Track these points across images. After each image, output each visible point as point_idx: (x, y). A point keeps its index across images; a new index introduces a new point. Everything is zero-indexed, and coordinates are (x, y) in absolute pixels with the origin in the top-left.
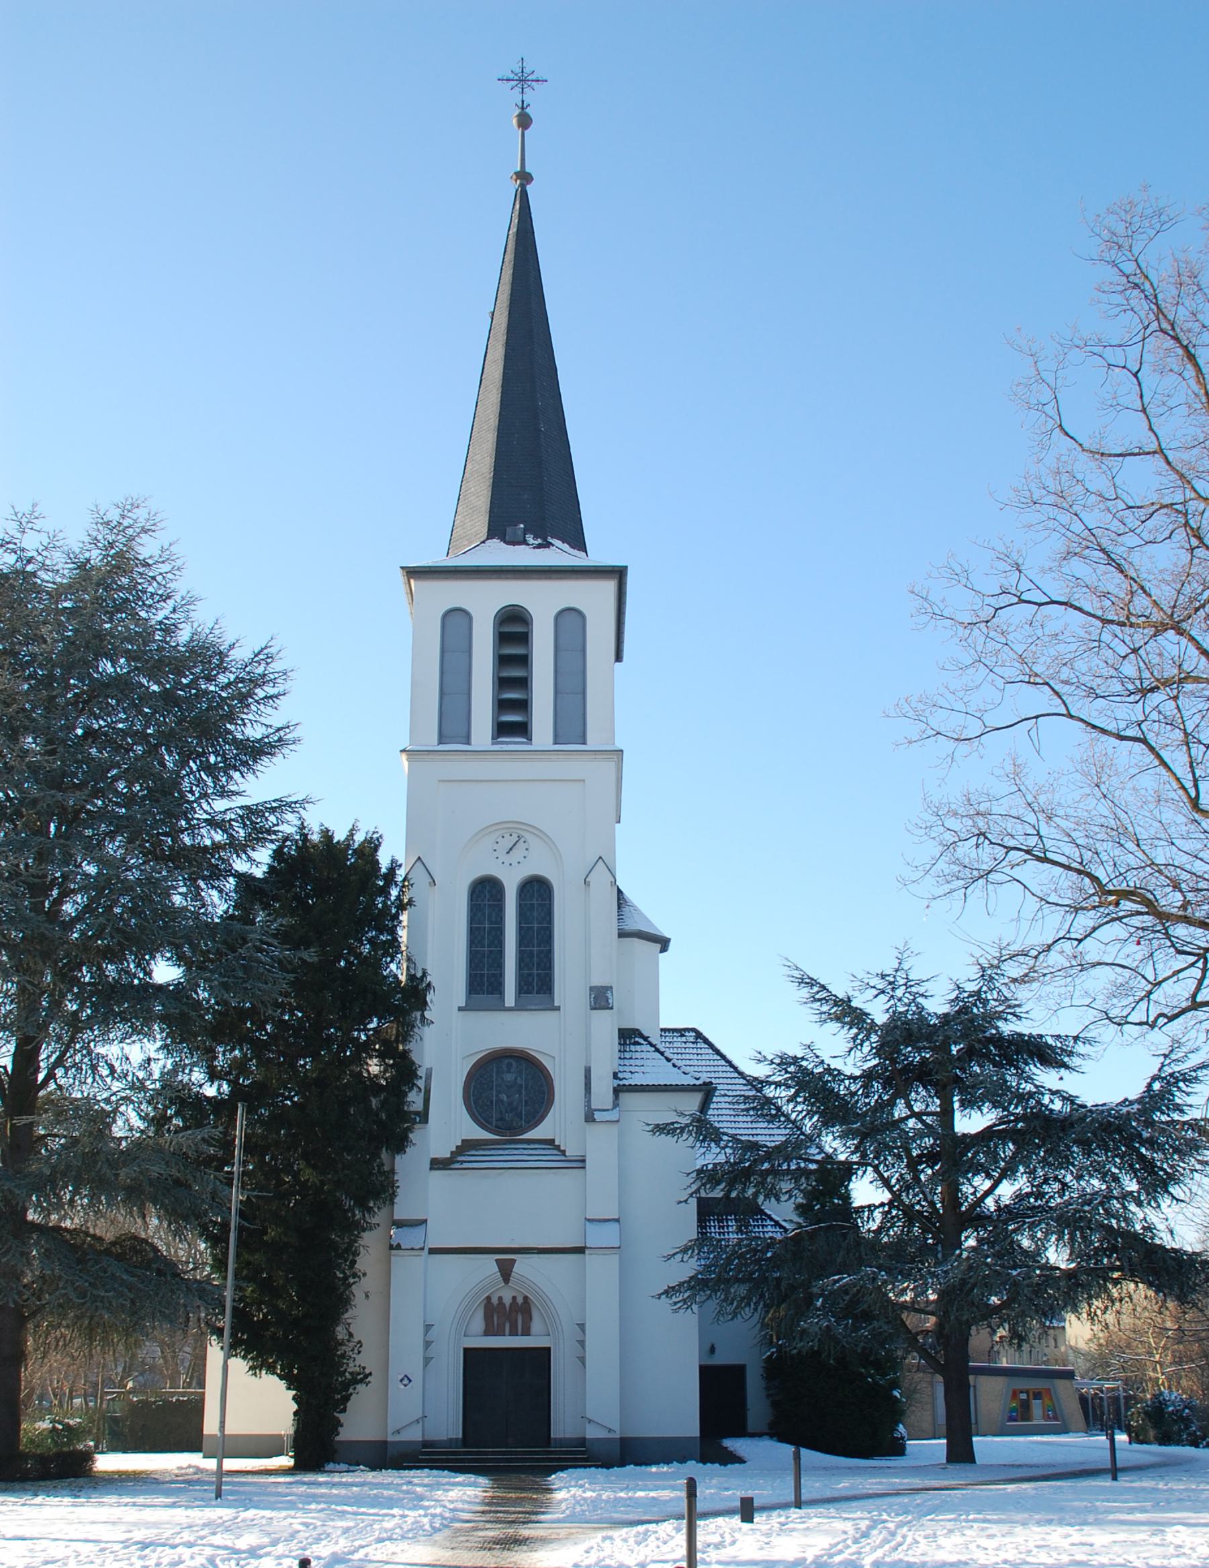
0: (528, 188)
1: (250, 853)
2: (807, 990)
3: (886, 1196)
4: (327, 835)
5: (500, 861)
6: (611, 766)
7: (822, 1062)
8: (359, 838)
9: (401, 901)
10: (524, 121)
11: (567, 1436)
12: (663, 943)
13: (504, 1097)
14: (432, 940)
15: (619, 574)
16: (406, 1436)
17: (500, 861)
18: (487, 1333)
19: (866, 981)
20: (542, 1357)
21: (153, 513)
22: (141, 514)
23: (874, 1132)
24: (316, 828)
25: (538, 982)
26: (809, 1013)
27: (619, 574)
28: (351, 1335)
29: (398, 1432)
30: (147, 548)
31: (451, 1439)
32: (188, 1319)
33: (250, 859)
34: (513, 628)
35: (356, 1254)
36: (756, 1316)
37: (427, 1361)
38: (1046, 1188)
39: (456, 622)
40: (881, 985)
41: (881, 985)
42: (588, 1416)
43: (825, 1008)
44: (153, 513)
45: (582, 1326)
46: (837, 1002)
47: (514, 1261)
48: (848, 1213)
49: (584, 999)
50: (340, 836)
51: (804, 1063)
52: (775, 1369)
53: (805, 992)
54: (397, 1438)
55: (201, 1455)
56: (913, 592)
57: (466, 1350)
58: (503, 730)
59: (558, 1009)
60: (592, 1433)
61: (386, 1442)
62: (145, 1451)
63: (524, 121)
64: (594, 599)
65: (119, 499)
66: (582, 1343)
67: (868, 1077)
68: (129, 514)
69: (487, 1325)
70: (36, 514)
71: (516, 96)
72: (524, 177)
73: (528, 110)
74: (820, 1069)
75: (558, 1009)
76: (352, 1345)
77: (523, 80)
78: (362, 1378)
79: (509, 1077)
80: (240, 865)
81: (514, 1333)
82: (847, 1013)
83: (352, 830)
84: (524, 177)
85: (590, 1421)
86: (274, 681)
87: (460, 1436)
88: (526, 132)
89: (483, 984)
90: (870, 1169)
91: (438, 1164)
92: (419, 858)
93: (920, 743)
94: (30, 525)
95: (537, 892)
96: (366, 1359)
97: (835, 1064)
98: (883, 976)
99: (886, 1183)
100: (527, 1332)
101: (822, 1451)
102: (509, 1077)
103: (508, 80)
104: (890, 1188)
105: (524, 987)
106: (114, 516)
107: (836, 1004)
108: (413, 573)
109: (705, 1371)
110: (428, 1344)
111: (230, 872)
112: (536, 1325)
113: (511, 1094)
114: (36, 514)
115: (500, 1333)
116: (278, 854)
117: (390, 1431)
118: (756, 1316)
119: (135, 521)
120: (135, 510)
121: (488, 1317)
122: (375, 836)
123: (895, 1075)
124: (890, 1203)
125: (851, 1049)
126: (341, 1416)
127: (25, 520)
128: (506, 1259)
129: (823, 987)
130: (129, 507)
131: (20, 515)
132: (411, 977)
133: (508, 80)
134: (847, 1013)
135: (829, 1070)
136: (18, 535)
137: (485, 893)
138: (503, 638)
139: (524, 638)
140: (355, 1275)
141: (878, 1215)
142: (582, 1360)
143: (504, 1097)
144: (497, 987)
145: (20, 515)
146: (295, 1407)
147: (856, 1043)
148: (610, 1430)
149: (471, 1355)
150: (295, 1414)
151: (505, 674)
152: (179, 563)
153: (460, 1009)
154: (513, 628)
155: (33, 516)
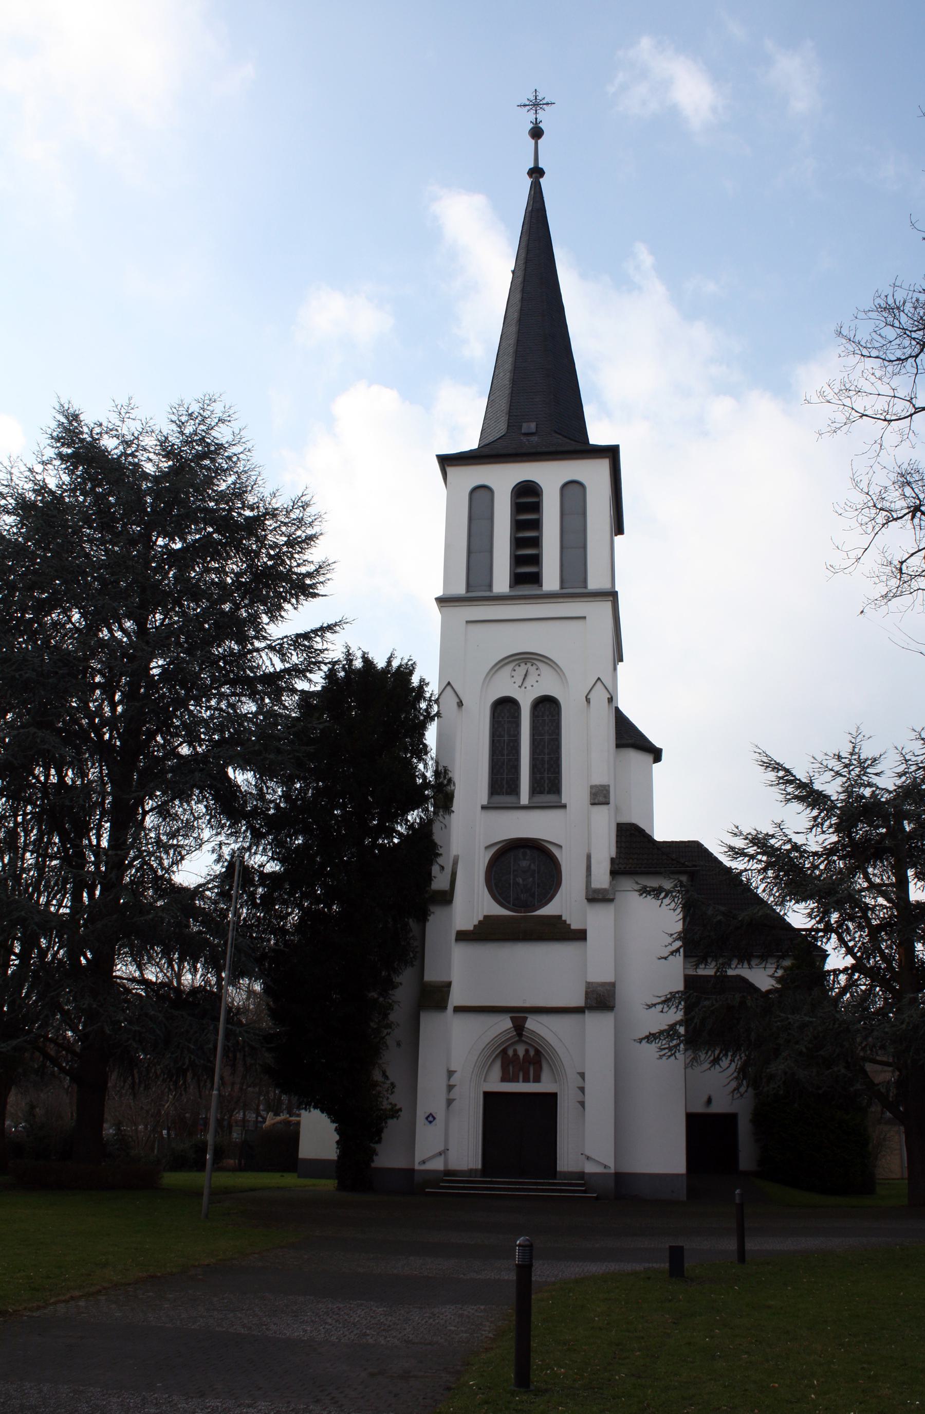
0: (541, 180)
1: (308, 674)
2: (774, 774)
3: (849, 961)
4: (366, 660)
6: (608, 606)
7: (790, 841)
8: (395, 664)
9: (429, 713)
10: (537, 133)
11: (571, 1169)
13: (520, 880)
14: (454, 745)
15: (612, 453)
18: (504, 1079)
19: (825, 763)
20: (550, 1100)
21: (227, 407)
22: (218, 409)
23: (831, 894)
24: (359, 654)
25: (548, 782)
26: (776, 794)
27: (612, 453)
28: (386, 1077)
29: (424, 1162)
30: (222, 434)
31: (471, 1170)
32: (235, 1058)
33: (310, 681)
34: (527, 498)
36: (733, 1065)
37: (450, 1102)
39: (481, 495)
40: (838, 767)
41: (838, 767)
42: (588, 1153)
43: (790, 789)
44: (227, 407)
45: (582, 1075)
46: (802, 786)
47: (526, 1018)
48: (820, 976)
49: (586, 797)
50: (381, 664)
51: (772, 841)
52: (760, 1118)
53: (772, 776)
54: (423, 1167)
55: (295, 1175)
56: (840, 333)
57: (487, 1095)
58: (518, 579)
59: (564, 806)
60: (590, 1168)
62: (324, 1160)
63: (537, 133)
64: (594, 474)
65: (200, 396)
66: (582, 1089)
67: (830, 852)
68: (209, 408)
70: (132, 406)
71: (531, 116)
72: (536, 173)
73: (540, 125)
74: (788, 847)
75: (564, 806)
76: (386, 1086)
77: (536, 104)
78: (395, 1112)
79: (524, 864)
80: (301, 685)
81: (526, 1080)
82: (809, 795)
83: (391, 657)
84: (536, 173)
85: (588, 1158)
86: (311, 524)
87: (480, 1167)
88: (539, 141)
89: (502, 784)
90: (834, 936)
91: (463, 936)
92: (449, 684)
93: (845, 428)
94: (128, 415)
95: (547, 708)
96: (398, 1098)
97: (799, 840)
98: (839, 758)
99: (850, 951)
100: (537, 1079)
102: (524, 864)
103: (525, 106)
104: (854, 956)
105: (535, 790)
106: (195, 408)
107: (798, 787)
108: (468, 622)
109: (691, 1119)
110: (450, 1088)
111: (294, 691)
112: (545, 1075)
113: (524, 871)
114: (132, 406)
115: (515, 1079)
116: (331, 676)
117: (418, 1159)
118: (733, 1065)
119: (212, 412)
120: (213, 404)
121: (504, 1068)
122: (410, 663)
123: (859, 853)
124: (854, 968)
125: (813, 826)
126: (377, 1146)
127: (123, 411)
128: (519, 1015)
129: (787, 771)
130: (207, 402)
131: (119, 407)
132: (437, 773)
133: (525, 106)
134: (809, 795)
135: (796, 847)
136: (120, 424)
137: (504, 709)
139: (536, 507)
140: (389, 1026)
141: (843, 978)
142: (582, 1104)
144: (514, 790)
145: (119, 407)
146: (337, 1137)
147: (816, 823)
148: (605, 1167)
149: (487, 1095)
150: (338, 1142)
151: (520, 535)
152: (249, 446)
153: (483, 808)
154: (527, 498)
155: (130, 407)
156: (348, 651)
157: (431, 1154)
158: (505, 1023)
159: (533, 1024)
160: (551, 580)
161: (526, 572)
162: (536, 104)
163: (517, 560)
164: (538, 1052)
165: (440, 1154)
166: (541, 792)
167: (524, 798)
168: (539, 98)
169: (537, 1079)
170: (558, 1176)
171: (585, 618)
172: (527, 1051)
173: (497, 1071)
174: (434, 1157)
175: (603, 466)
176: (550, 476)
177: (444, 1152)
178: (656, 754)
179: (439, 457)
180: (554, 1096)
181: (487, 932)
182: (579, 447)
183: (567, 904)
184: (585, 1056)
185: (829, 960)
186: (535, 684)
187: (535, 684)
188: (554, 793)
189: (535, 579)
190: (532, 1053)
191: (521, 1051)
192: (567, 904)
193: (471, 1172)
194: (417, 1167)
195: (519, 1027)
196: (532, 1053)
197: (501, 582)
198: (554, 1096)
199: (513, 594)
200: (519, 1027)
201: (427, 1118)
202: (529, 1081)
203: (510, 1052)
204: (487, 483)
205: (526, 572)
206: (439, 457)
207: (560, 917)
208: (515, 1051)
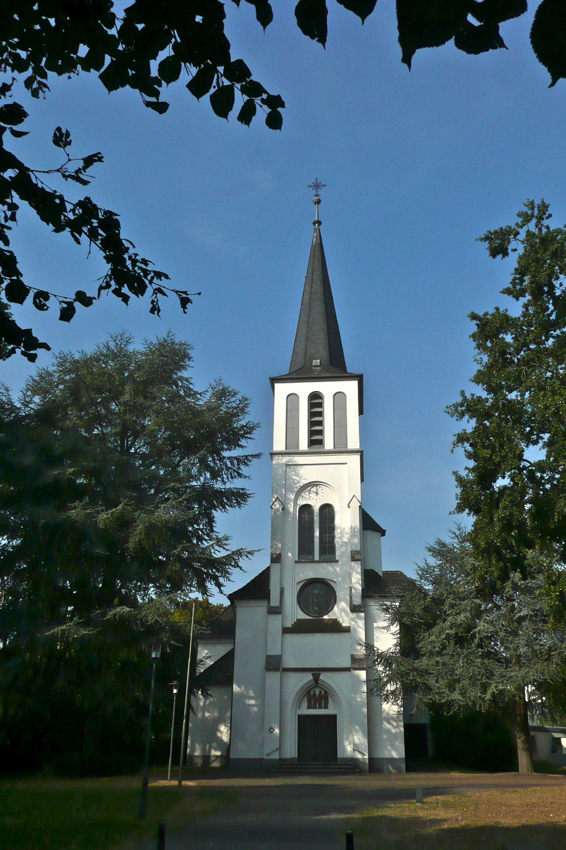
5: (315, 499)
12: (383, 533)
13: (315, 600)
16: (272, 757)
17: (315, 499)
18: (309, 707)
20: (333, 718)
25: (329, 551)
29: (268, 755)
34: (316, 400)
35: (475, 428)
38: (469, 567)
47: (320, 674)
57: (301, 718)
58: (311, 443)
61: (263, 759)
69: (308, 704)
77: (317, 186)
79: (316, 592)
81: (320, 707)
87: (297, 756)
89: (305, 551)
100: (326, 707)
101: (333, 300)
102: (316, 592)
105: (322, 551)
108: (346, 464)
117: (265, 754)
128: (316, 672)
138: (311, 405)
139: (321, 405)
143: (315, 600)
144: (312, 552)
149: (301, 718)
153: (296, 562)
154: (316, 400)
156: (458, 442)
157: (272, 750)
158: (309, 677)
159: (323, 677)
160: (329, 444)
161: (316, 439)
162: (317, 186)
163: (311, 433)
164: (326, 692)
165: (277, 750)
166: (325, 554)
167: (317, 558)
168: (319, 182)
169: (326, 707)
170: (338, 761)
171: (346, 464)
172: (320, 692)
173: (305, 704)
174: (273, 751)
175: (354, 384)
176: (328, 389)
177: (280, 749)
178: (383, 533)
179: (270, 378)
180: (335, 716)
181: (300, 628)
182: (345, 450)
183: (340, 612)
184: (351, 690)
185: (55, 74)
186: (321, 498)
187: (321, 498)
188: (332, 554)
189: (321, 442)
190: (323, 693)
191: (317, 693)
192: (340, 612)
193: (292, 759)
194: (265, 758)
195: (316, 678)
196: (323, 693)
197: (303, 445)
198: (335, 716)
199: (310, 451)
200: (316, 678)
201: (270, 730)
202: (321, 708)
203: (312, 693)
204: (295, 392)
205: (316, 439)
206: (270, 378)
207: (336, 619)
208: (314, 692)
